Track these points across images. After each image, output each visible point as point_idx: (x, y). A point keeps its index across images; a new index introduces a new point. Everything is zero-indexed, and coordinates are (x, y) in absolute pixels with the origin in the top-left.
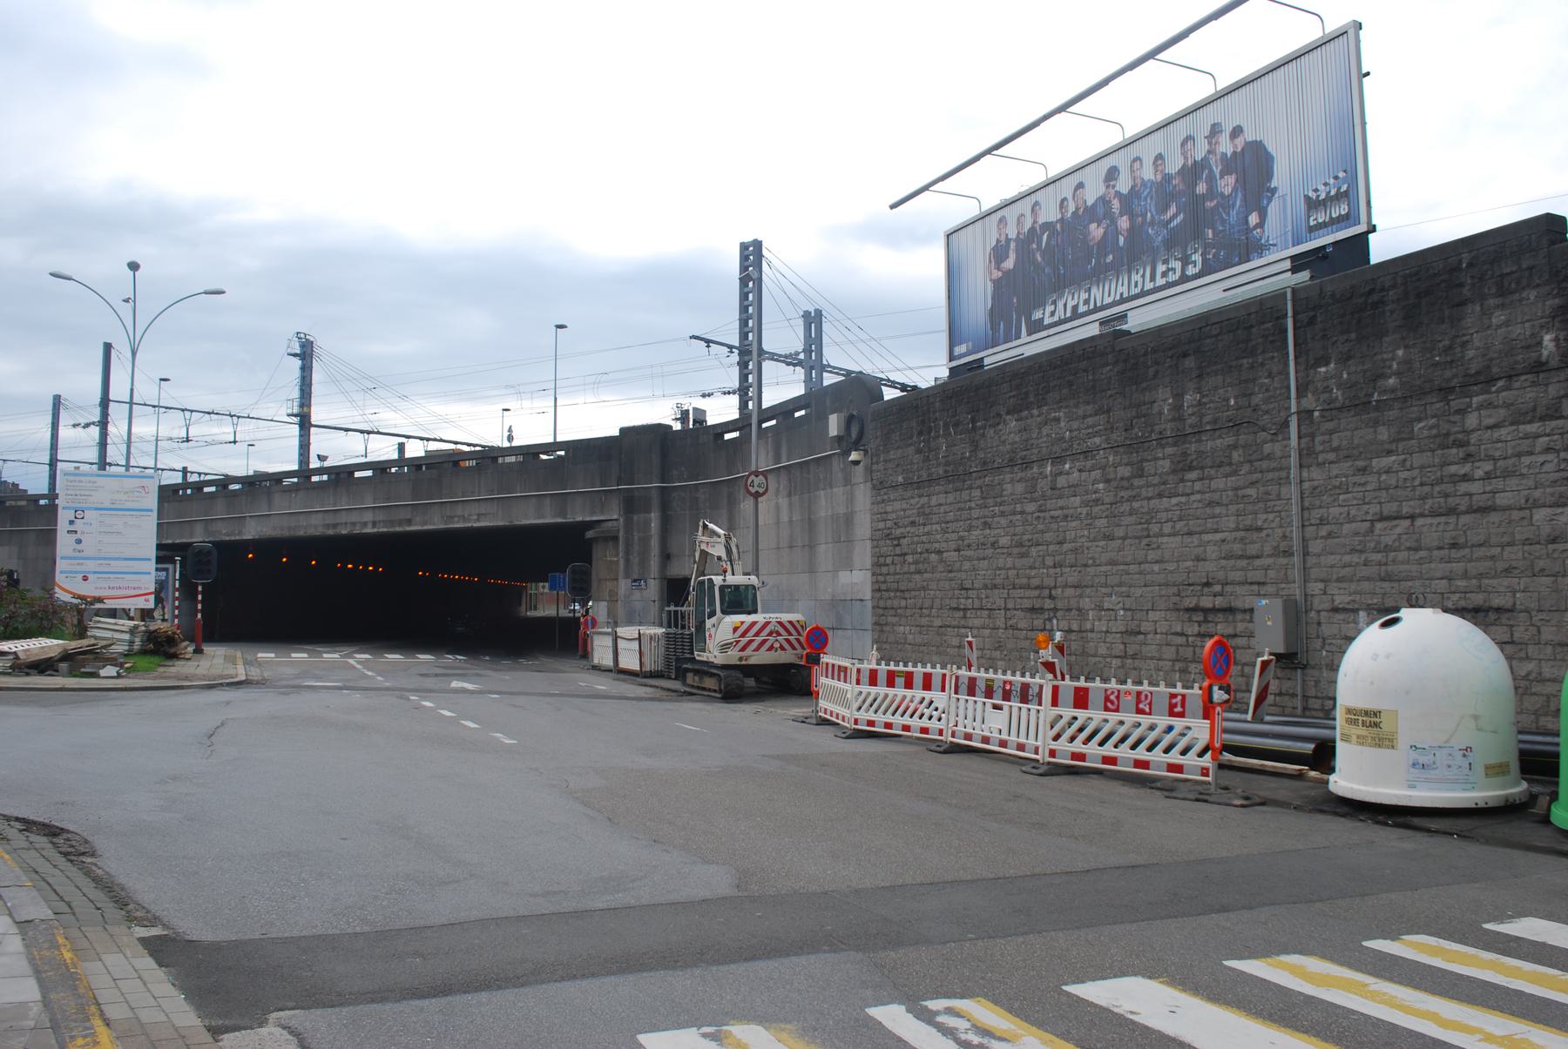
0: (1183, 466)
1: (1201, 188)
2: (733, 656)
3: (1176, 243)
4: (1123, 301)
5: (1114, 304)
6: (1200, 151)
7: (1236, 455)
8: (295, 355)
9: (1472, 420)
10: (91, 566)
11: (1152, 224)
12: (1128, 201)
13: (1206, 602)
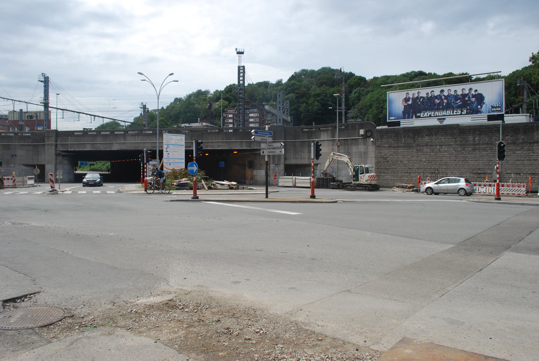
0: (474, 150)
1: (467, 99)
2: (369, 182)
3: (461, 107)
4: (444, 116)
5: (442, 116)
6: (467, 92)
7: (487, 149)
8: (42, 81)
9: (534, 148)
10: (171, 161)
11: (453, 103)
12: (446, 97)
13: (479, 172)
